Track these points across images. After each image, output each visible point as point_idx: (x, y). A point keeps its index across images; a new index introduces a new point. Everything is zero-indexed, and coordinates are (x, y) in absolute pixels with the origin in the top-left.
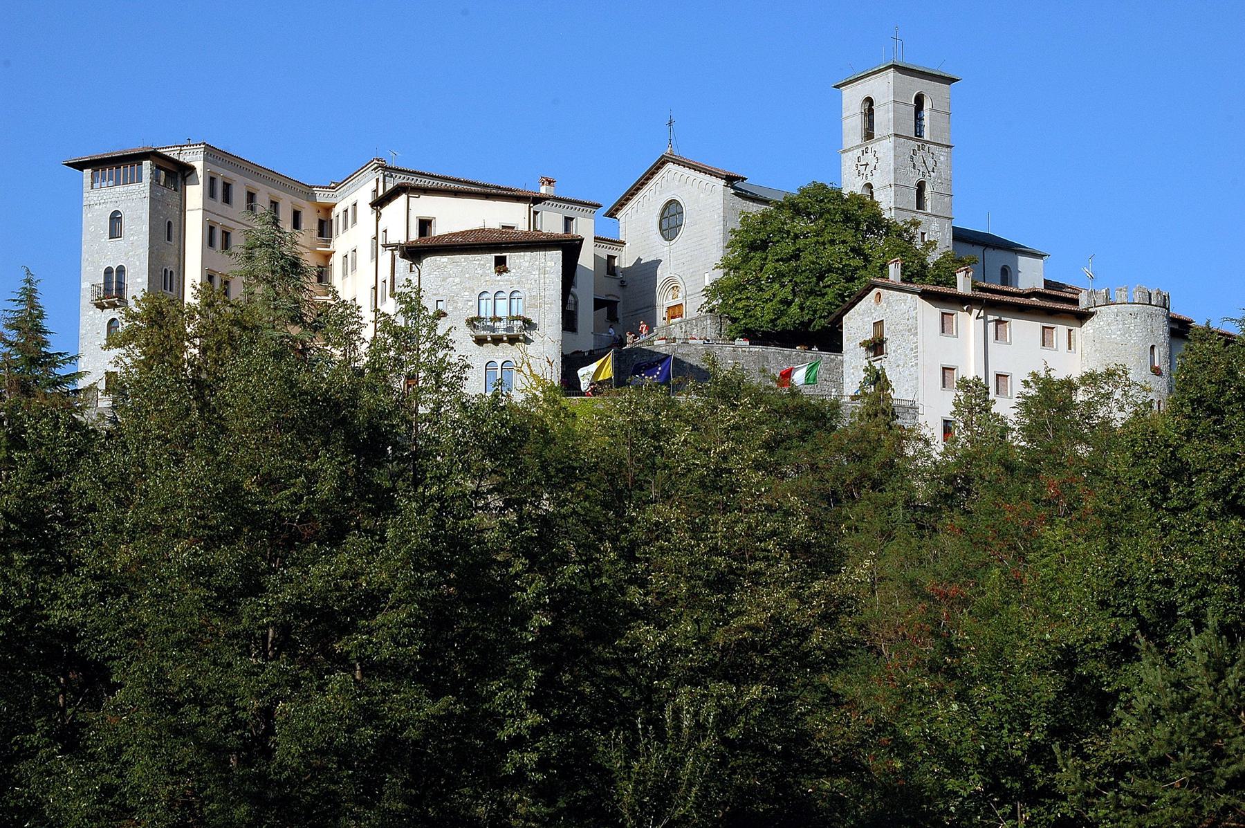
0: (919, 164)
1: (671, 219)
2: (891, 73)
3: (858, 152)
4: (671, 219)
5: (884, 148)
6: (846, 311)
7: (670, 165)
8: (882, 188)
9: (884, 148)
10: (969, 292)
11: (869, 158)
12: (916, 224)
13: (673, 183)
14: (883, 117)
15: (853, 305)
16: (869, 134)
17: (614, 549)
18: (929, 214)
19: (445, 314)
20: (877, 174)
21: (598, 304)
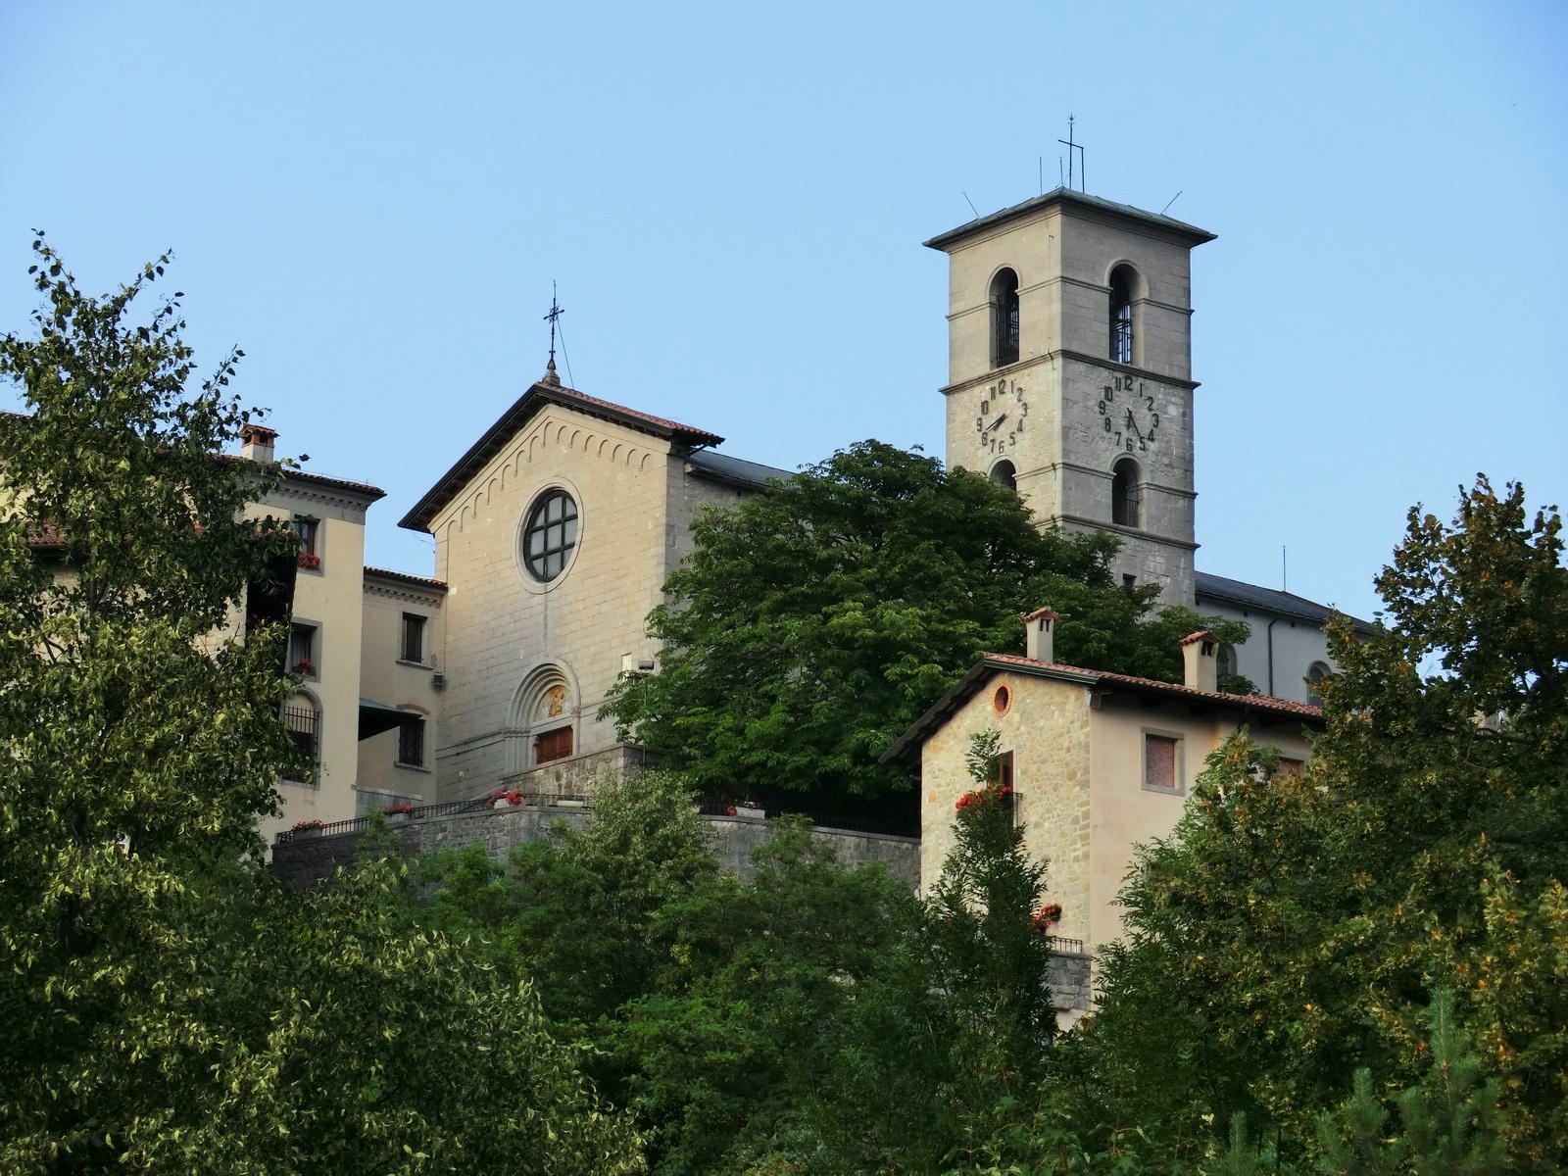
0: (1119, 422)
1: (547, 530)
2: (1055, 221)
3: (982, 392)
4: (547, 530)
5: (1042, 386)
6: (931, 731)
7: (551, 413)
8: (1037, 472)
9: (1042, 386)
10: (1210, 689)
11: (1008, 402)
12: (1110, 549)
13: (552, 451)
14: (1041, 319)
15: (946, 716)
16: (1006, 350)
17: (816, 657)
18: (1141, 536)
19: (406, 523)
20: (1024, 440)
21: (372, 721)
